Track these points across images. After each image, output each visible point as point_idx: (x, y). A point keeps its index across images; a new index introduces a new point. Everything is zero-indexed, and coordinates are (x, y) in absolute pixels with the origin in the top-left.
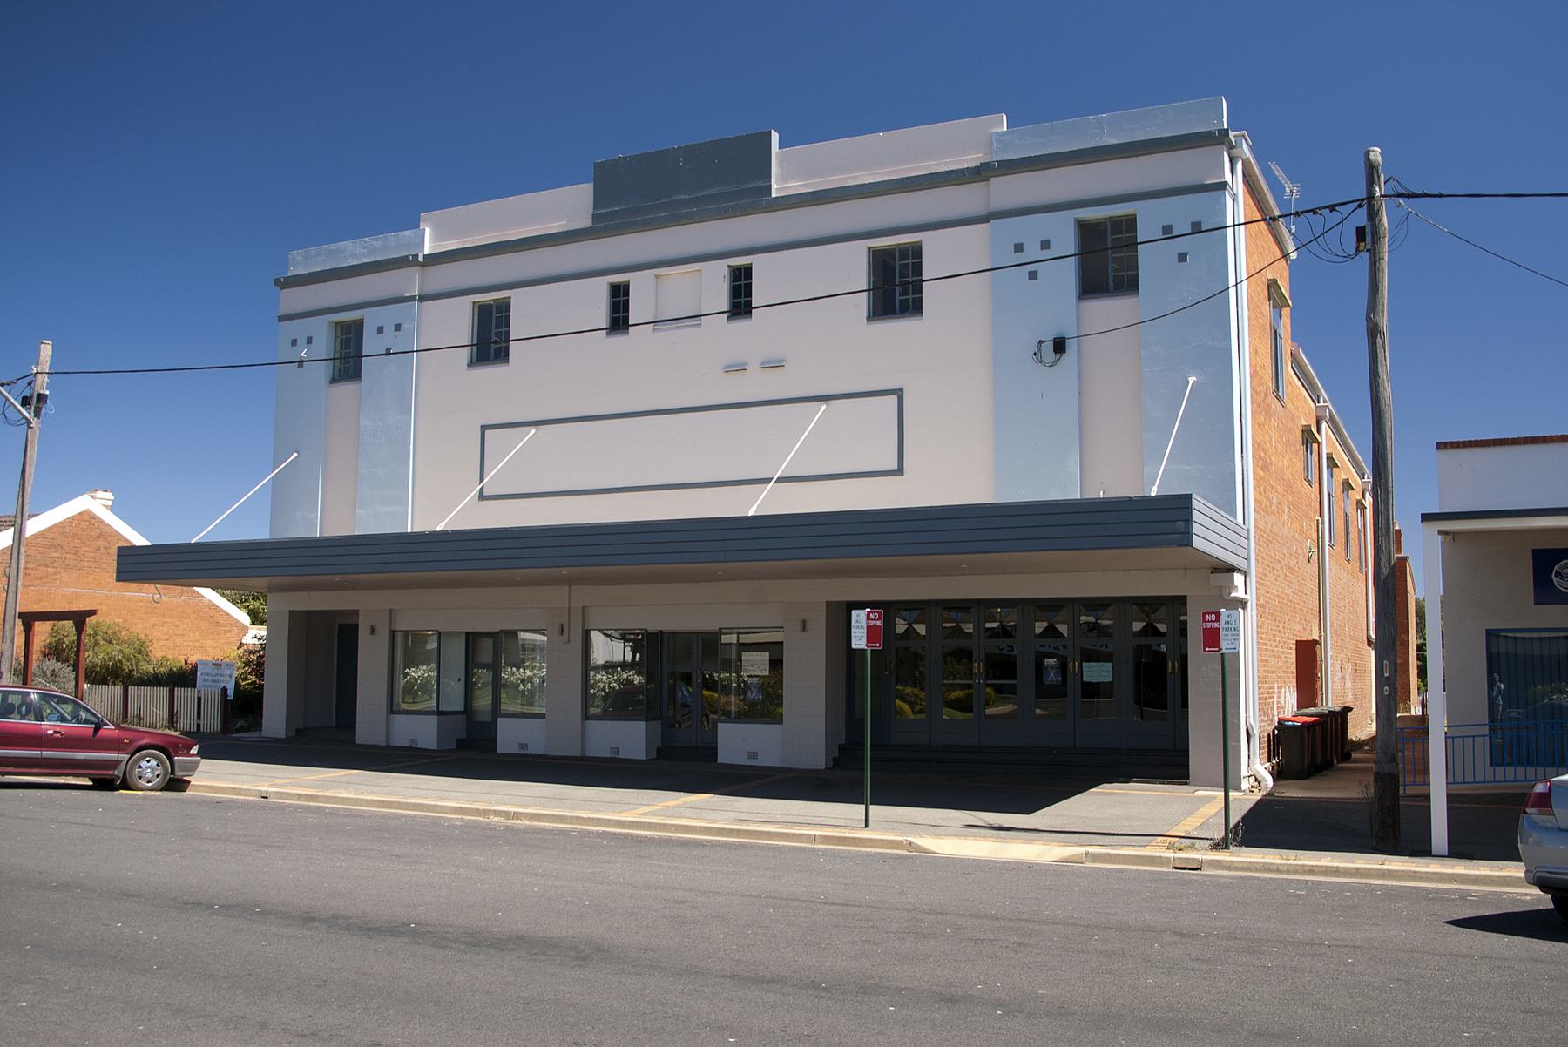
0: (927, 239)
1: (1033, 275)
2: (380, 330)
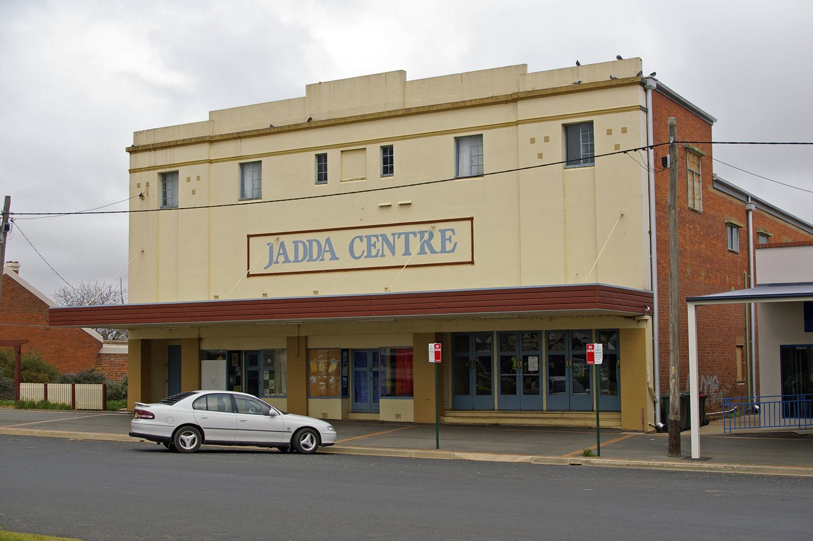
0: (596, 120)
1: (617, 147)
2: (188, 180)
